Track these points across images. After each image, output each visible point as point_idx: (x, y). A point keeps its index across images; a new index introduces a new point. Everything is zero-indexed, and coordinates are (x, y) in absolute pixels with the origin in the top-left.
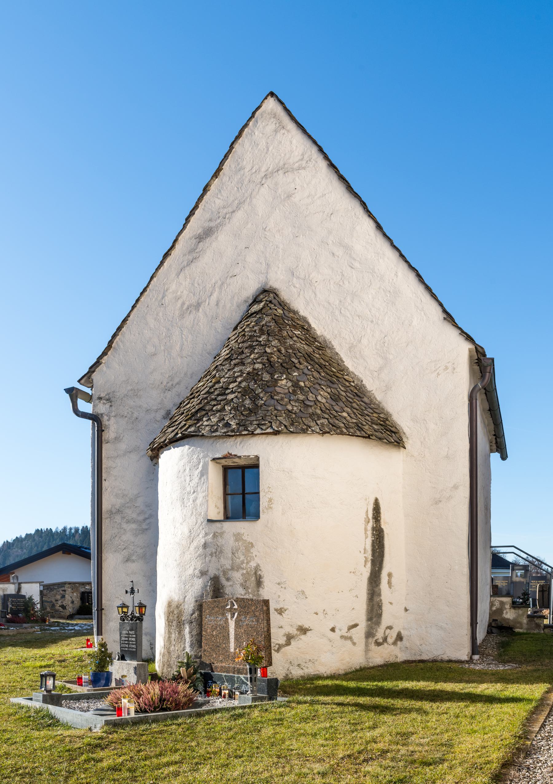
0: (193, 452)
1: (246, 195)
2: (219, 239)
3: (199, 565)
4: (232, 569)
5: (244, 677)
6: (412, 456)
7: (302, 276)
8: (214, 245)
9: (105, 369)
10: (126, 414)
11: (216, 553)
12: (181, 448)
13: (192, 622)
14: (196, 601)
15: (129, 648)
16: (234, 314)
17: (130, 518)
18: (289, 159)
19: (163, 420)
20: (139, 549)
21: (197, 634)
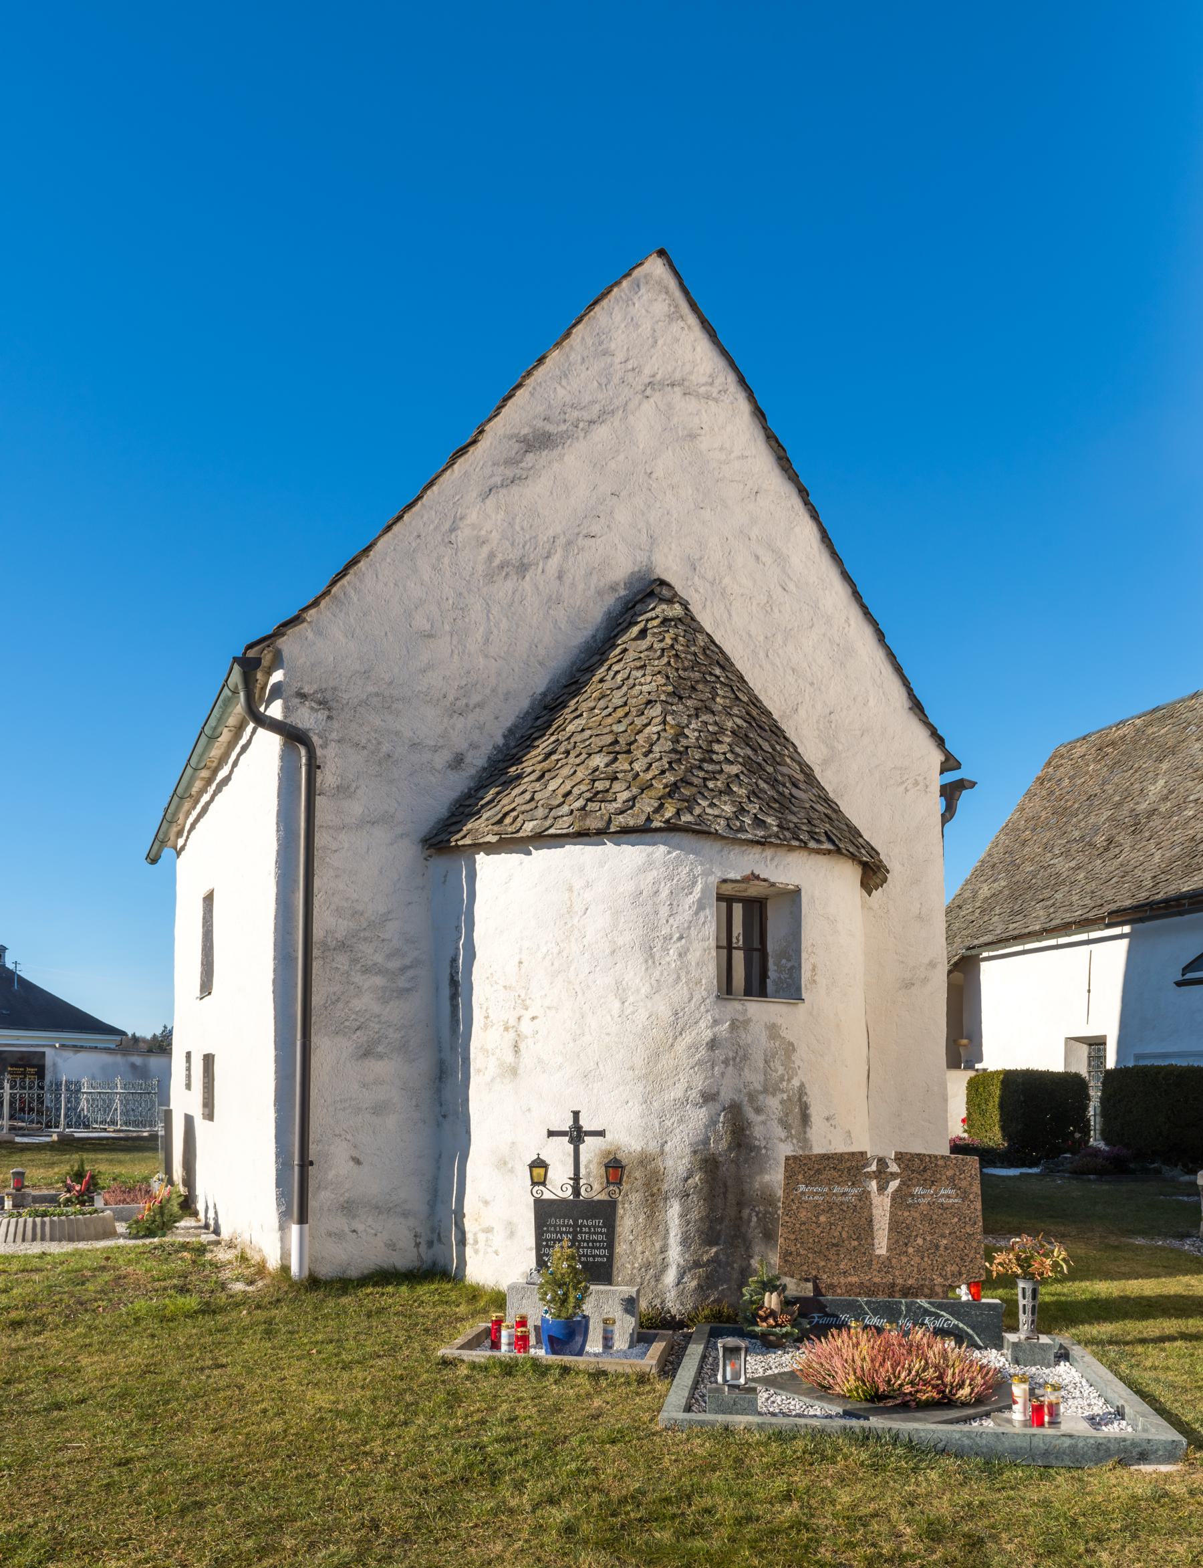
0: (678, 862)
1: (617, 402)
2: (566, 458)
3: (699, 1083)
4: (765, 1091)
6: (871, 908)
8: (556, 466)
9: (310, 635)
10: (364, 741)
11: (734, 1059)
12: (650, 849)
13: (688, 1195)
14: (695, 1152)
15: (594, 1256)
16: (591, 605)
17: (370, 963)
18: (691, 373)
20: (391, 1030)
21: (701, 1219)
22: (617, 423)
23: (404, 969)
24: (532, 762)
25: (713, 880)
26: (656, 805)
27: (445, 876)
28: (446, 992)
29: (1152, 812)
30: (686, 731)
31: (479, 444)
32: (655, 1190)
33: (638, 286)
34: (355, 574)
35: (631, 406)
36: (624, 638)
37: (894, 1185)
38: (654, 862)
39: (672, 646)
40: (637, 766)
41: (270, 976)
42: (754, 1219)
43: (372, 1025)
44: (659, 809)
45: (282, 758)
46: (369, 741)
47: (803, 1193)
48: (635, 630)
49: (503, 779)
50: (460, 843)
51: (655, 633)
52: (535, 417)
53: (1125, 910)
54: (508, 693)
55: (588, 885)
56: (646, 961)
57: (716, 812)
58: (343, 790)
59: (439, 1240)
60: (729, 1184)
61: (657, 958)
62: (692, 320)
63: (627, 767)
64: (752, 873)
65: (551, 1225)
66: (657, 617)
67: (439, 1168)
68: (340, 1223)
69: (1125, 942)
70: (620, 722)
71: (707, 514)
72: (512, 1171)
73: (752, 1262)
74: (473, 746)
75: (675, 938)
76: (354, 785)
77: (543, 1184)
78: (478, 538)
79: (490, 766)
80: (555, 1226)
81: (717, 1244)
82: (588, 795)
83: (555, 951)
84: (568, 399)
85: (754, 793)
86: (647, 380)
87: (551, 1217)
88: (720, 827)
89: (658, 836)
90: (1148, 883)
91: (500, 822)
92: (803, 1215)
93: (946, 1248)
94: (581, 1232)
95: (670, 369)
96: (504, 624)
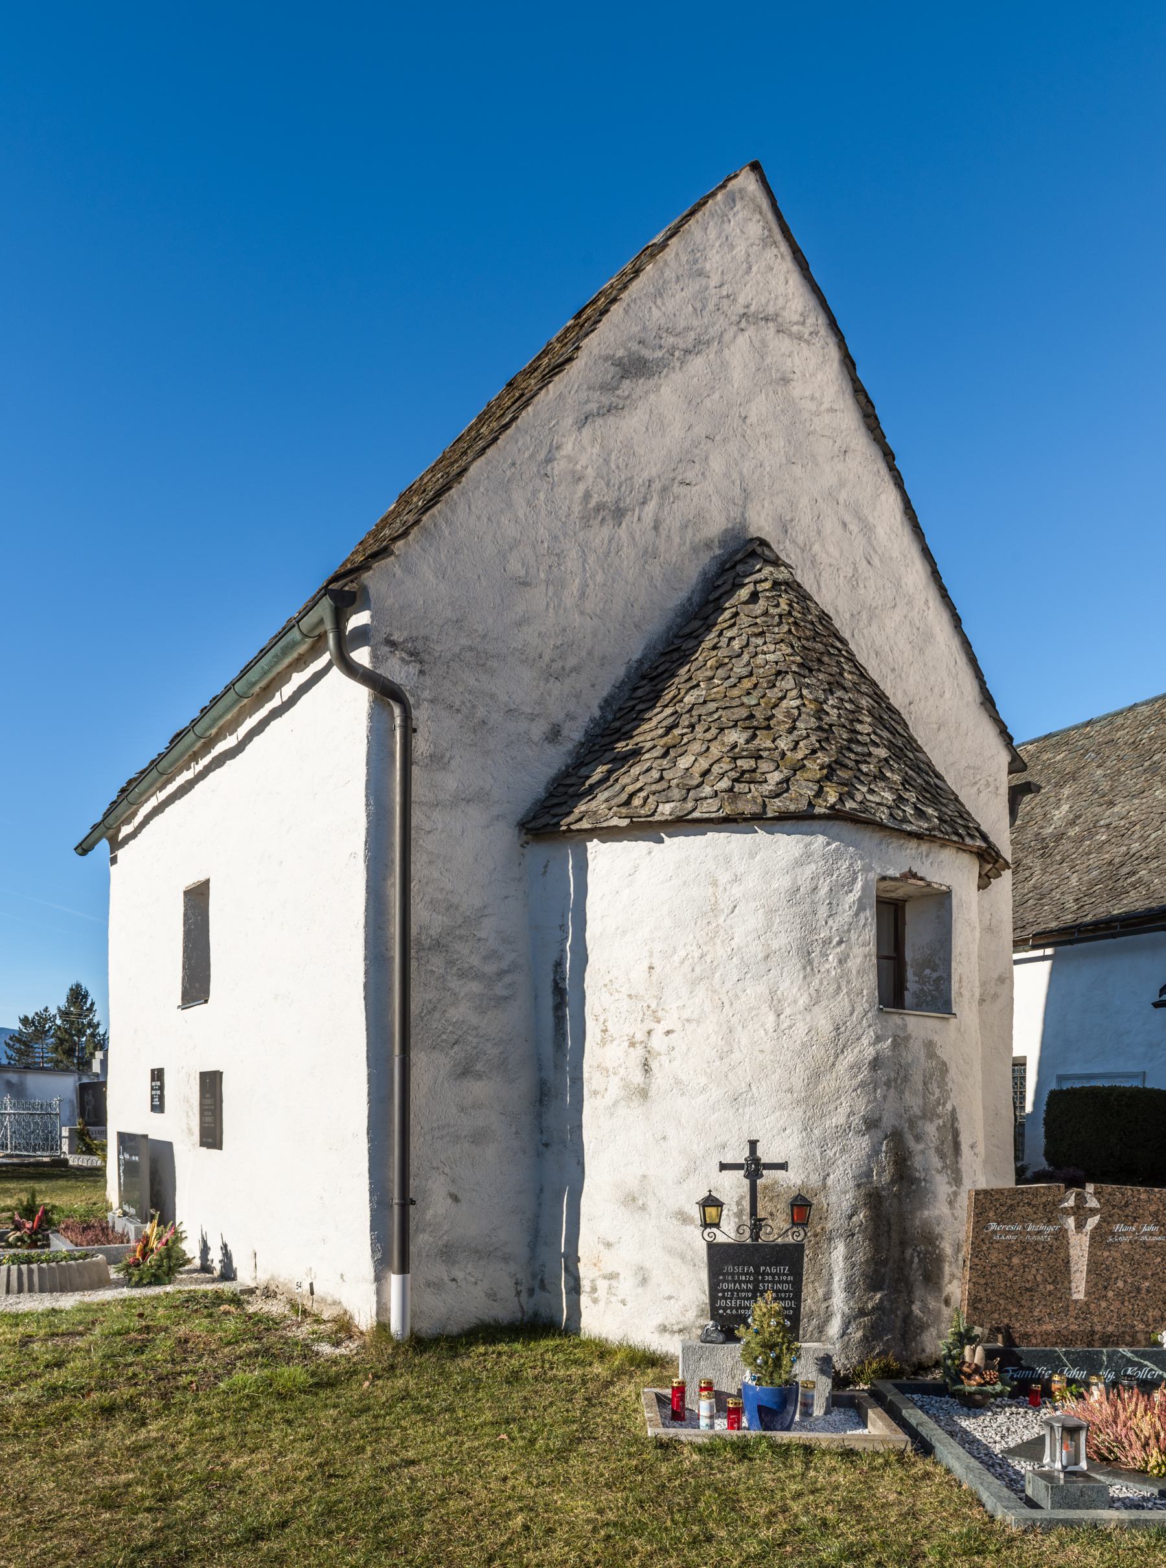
0: (838, 855)
1: (712, 332)
2: (662, 390)
3: (862, 1107)
4: (924, 1117)
5: (1132, 1352)
7: (800, 539)
9: (398, 571)
10: (458, 703)
11: (895, 1080)
12: (808, 839)
13: (853, 1235)
14: (859, 1186)
18: (783, 308)
19: (546, 744)
20: (489, 1045)
21: (867, 1261)
22: (712, 356)
23: (501, 974)
24: (648, 733)
25: (873, 876)
26: (816, 788)
27: (546, 867)
28: (548, 1001)
29: (1059, 837)
30: (825, 707)
31: (574, 363)
32: (819, 1230)
33: (734, 201)
34: (447, 503)
35: (727, 337)
36: (732, 601)
37: (1092, 1222)
38: (812, 854)
39: (790, 613)
40: (783, 744)
41: (361, 979)
42: (916, 1260)
43: (470, 1038)
44: (820, 793)
45: (371, 717)
46: (463, 703)
47: (994, 1232)
48: (744, 593)
49: (609, 755)
50: (573, 827)
51: (768, 598)
52: (630, 339)
53: (1051, 931)
54: (604, 658)
55: (736, 879)
56: (805, 968)
57: (878, 800)
58: (437, 760)
59: (543, 1286)
60: (892, 1221)
61: (815, 964)
62: (784, 248)
63: (769, 744)
64: (910, 871)
65: (728, 1274)
66: (766, 579)
67: (540, 1205)
68: (439, 1271)
69: (1047, 964)
70: (749, 694)
71: (797, 470)
72: (643, 1208)
73: (914, 1307)
74: (570, 717)
75: (834, 942)
76: (448, 755)
77: (717, 1225)
78: (573, 472)
79: (588, 741)
80: (733, 1274)
81: (881, 1289)
82: (734, 774)
83: (697, 954)
84: (662, 321)
85: (906, 780)
86: (742, 311)
87: (727, 1263)
88: (883, 815)
89: (816, 824)
90: (1071, 905)
91: (627, 803)
92: (994, 1257)
93: (1148, 1291)
94: (763, 1281)
95: (763, 301)
96: (600, 578)
